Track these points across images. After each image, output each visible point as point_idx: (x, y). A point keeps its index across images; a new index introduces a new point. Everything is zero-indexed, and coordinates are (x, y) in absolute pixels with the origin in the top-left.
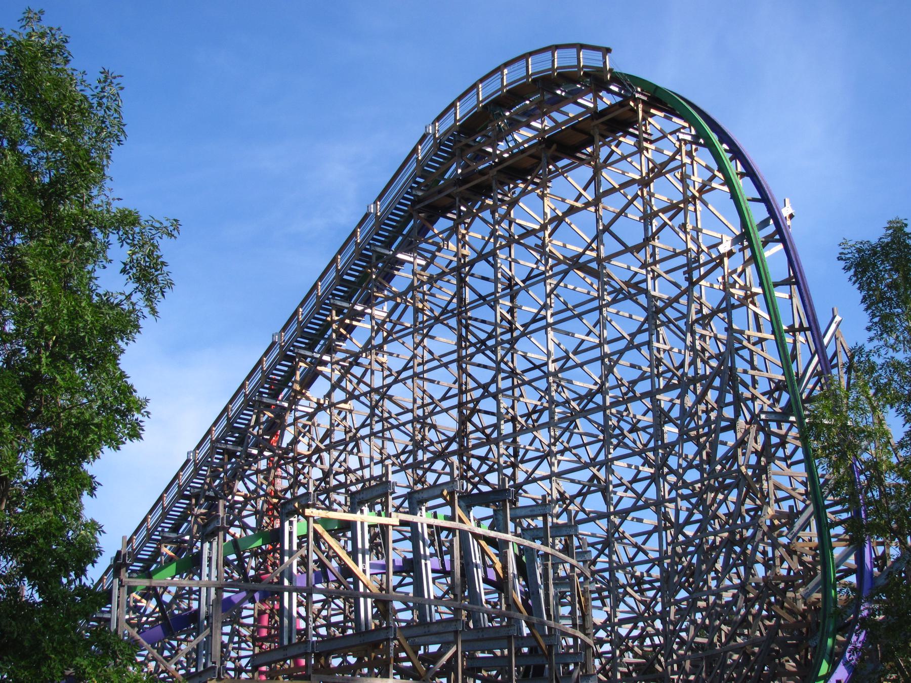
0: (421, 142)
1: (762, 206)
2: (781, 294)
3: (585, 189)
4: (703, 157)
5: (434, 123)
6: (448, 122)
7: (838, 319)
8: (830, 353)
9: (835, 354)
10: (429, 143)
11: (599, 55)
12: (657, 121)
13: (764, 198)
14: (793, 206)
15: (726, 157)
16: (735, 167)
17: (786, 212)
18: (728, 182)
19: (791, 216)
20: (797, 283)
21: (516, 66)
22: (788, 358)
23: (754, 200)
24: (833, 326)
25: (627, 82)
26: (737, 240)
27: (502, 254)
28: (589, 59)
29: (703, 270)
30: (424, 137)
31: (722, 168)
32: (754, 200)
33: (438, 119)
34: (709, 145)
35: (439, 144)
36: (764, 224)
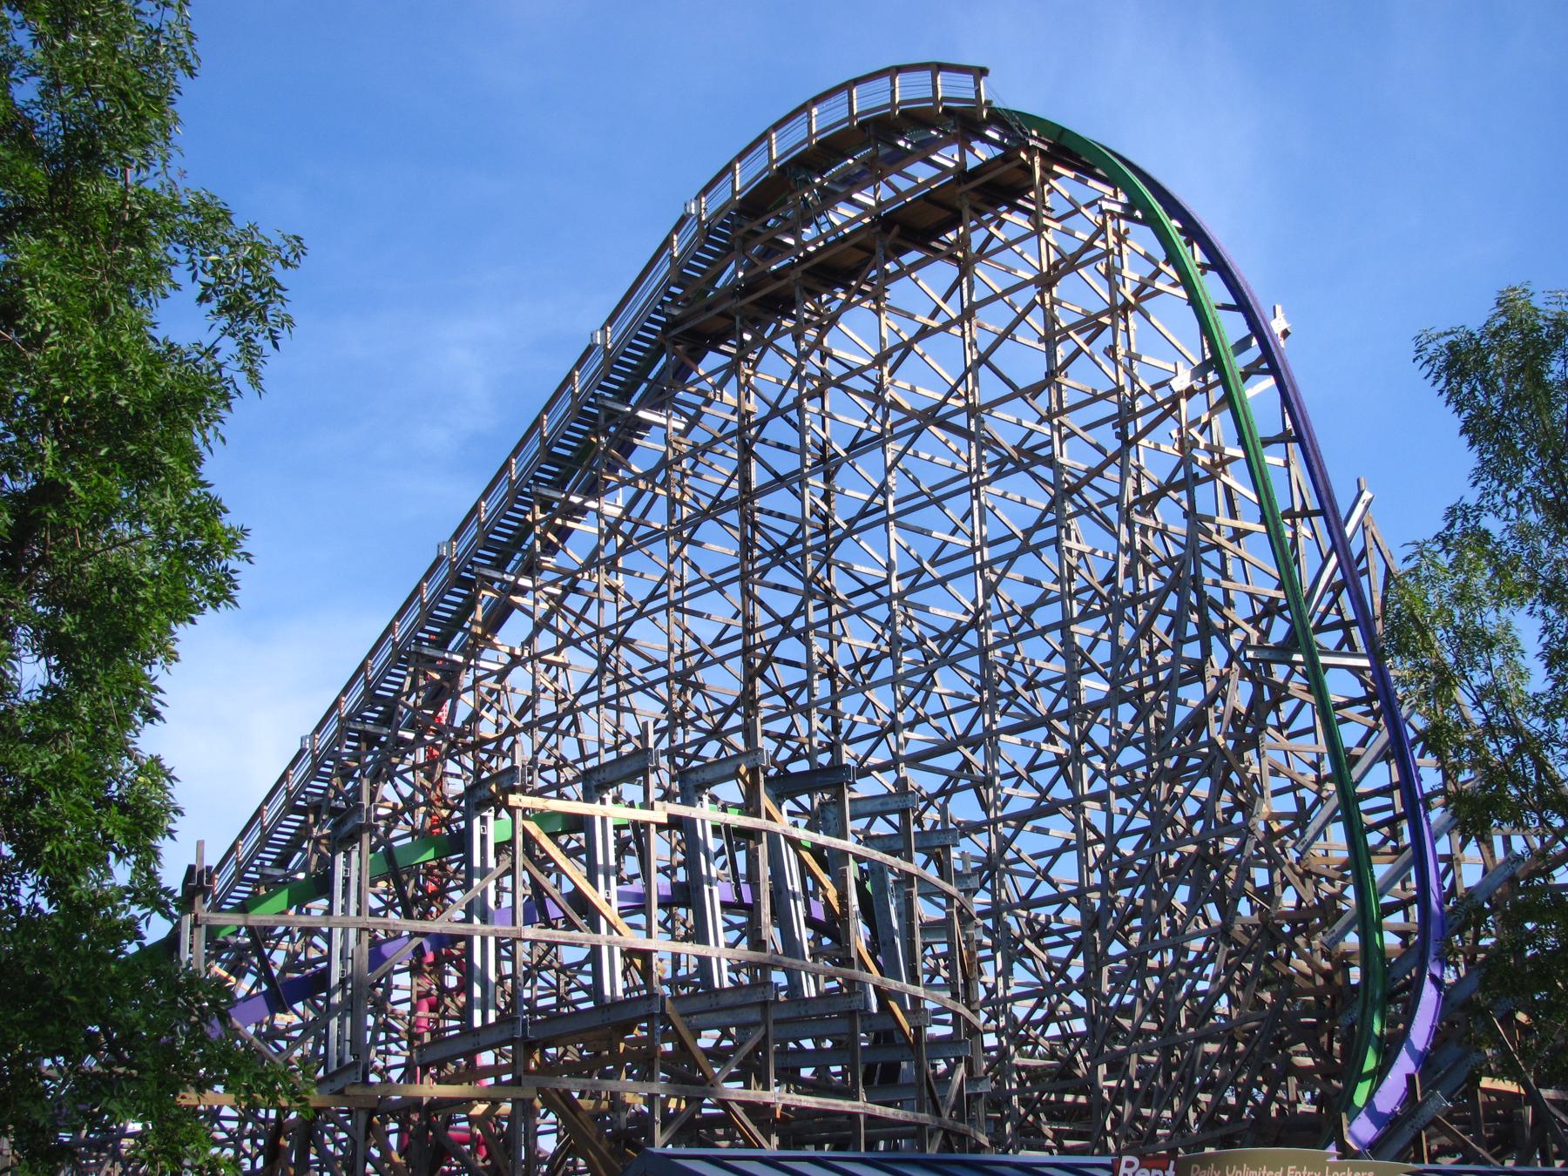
0: (677, 229)
1: (1239, 318)
2: (1272, 458)
3: (946, 299)
4: (1141, 240)
5: (698, 198)
6: (722, 195)
7: (1367, 496)
8: (1356, 551)
9: (1364, 553)
10: (691, 230)
11: (969, 79)
12: (1065, 185)
13: (1242, 304)
14: (1287, 318)
15: (1179, 240)
16: (1195, 256)
17: (1278, 325)
18: (1185, 281)
19: (1285, 334)
20: (1299, 439)
21: (832, 101)
22: (1285, 556)
23: (1225, 307)
24: (1360, 508)
25: (1011, 123)
26: (1200, 371)
27: (812, 407)
28: (953, 88)
29: (1141, 423)
30: (683, 220)
31: (1173, 258)
32: (1225, 307)
33: (705, 191)
34: (1151, 220)
35: (707, 232)
36: (1242, 345)
